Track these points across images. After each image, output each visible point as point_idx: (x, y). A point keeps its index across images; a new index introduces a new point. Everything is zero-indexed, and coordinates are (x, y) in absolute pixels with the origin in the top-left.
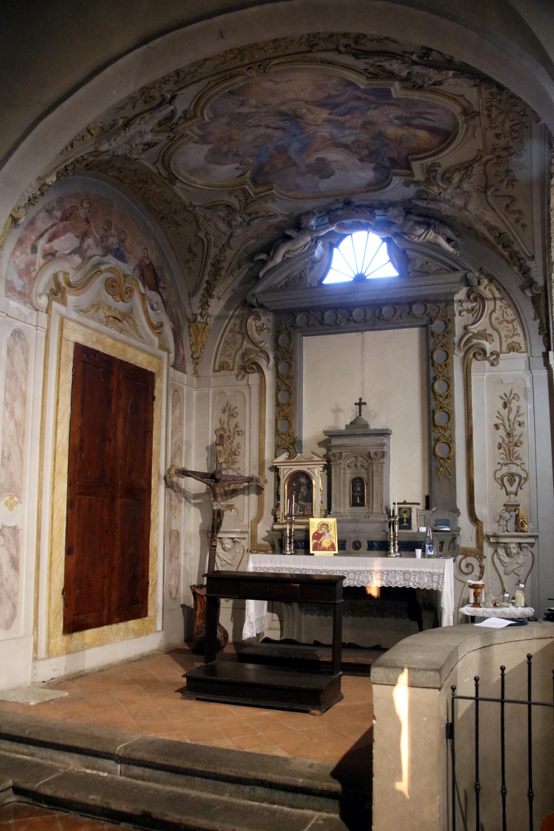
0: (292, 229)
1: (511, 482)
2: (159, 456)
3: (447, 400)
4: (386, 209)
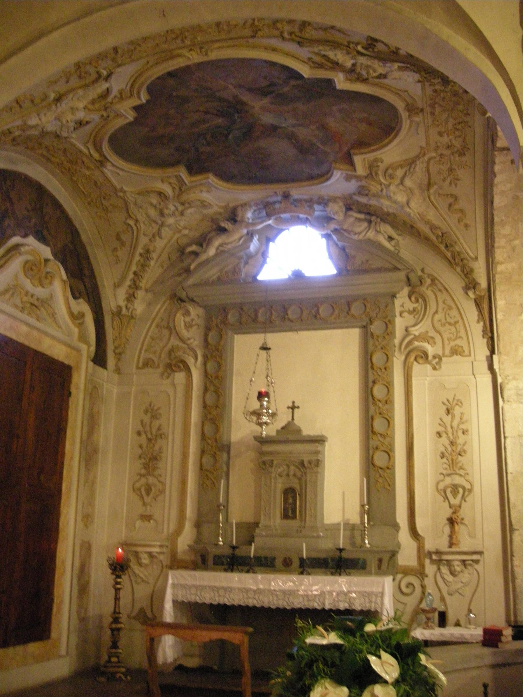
0: (227, 220)
1: (455, 493)
2: (72, 459)
3: (387, 406)
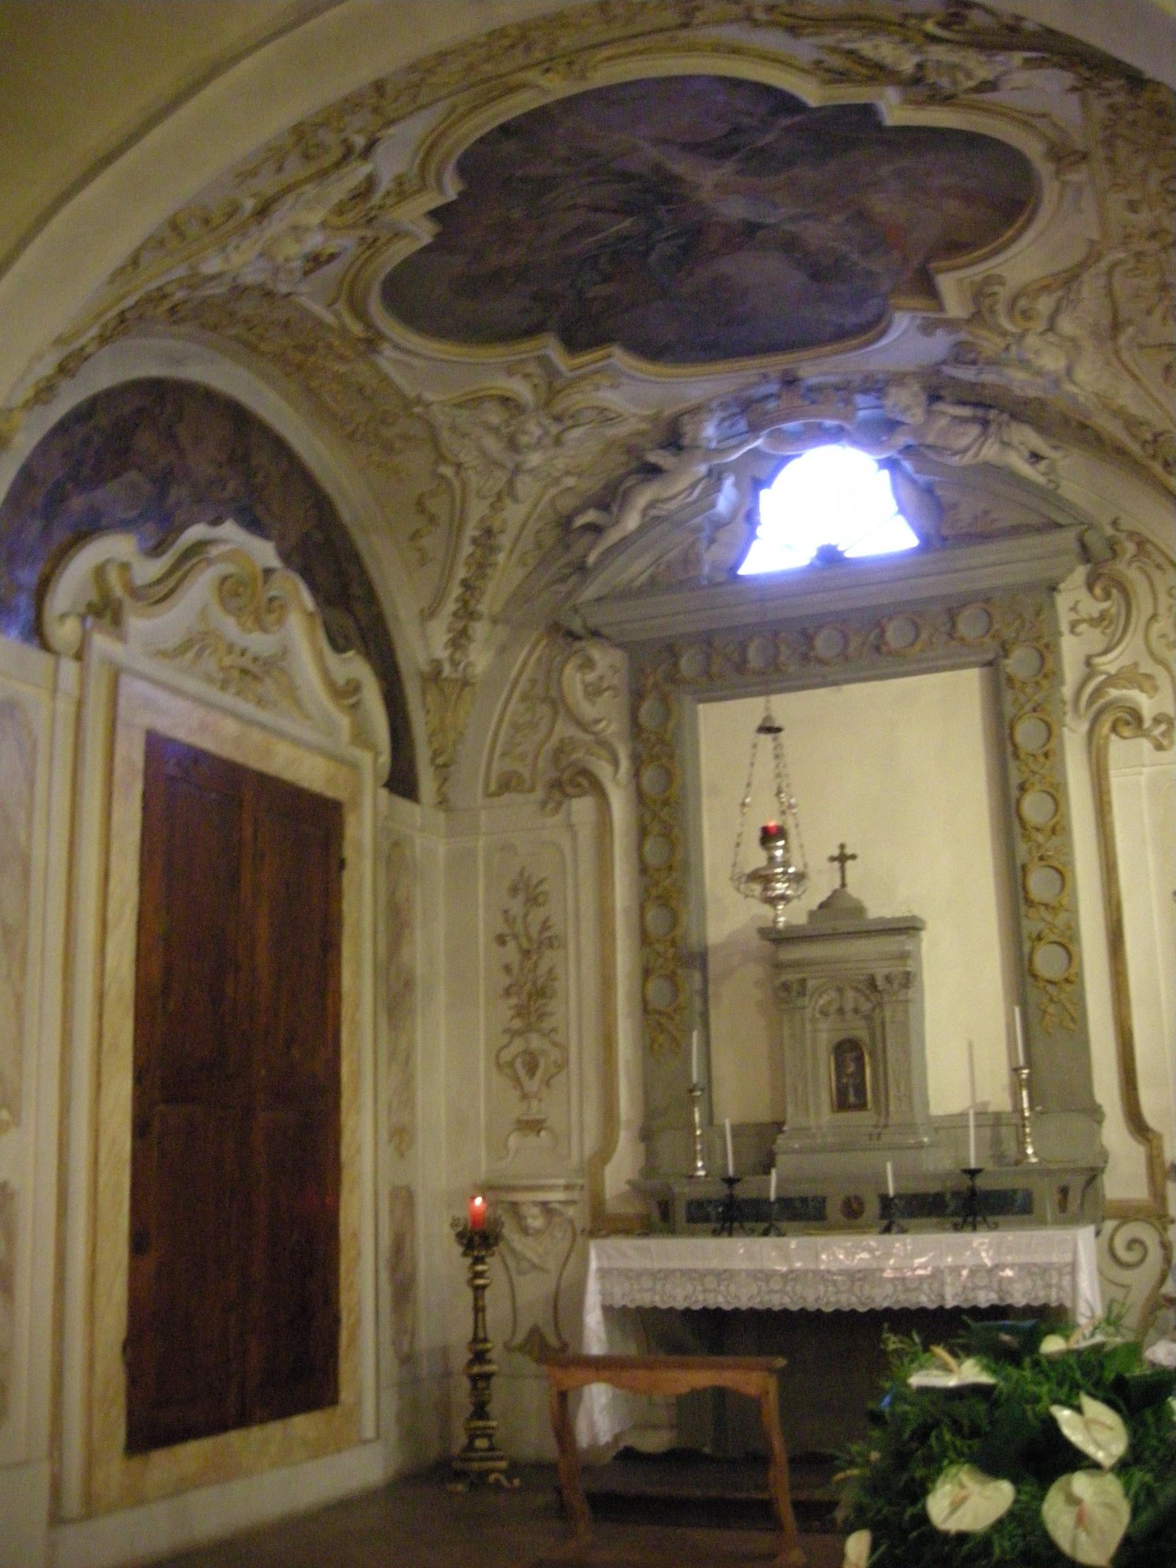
2: (357, 1006)
4: (880, 390)
